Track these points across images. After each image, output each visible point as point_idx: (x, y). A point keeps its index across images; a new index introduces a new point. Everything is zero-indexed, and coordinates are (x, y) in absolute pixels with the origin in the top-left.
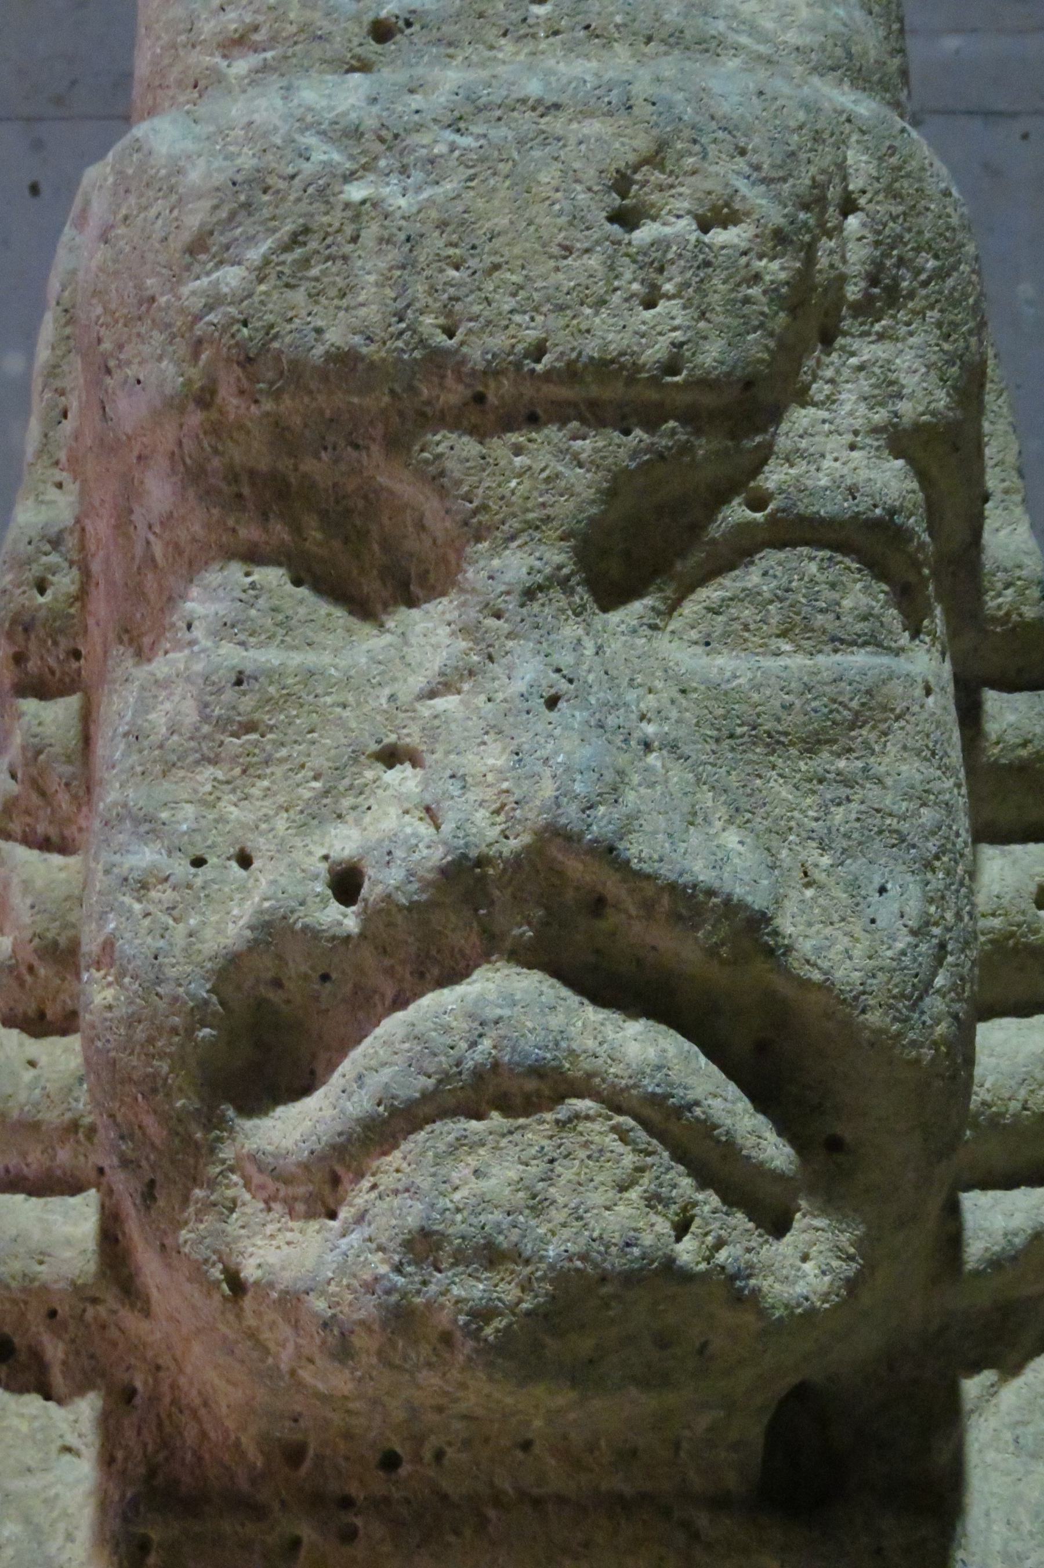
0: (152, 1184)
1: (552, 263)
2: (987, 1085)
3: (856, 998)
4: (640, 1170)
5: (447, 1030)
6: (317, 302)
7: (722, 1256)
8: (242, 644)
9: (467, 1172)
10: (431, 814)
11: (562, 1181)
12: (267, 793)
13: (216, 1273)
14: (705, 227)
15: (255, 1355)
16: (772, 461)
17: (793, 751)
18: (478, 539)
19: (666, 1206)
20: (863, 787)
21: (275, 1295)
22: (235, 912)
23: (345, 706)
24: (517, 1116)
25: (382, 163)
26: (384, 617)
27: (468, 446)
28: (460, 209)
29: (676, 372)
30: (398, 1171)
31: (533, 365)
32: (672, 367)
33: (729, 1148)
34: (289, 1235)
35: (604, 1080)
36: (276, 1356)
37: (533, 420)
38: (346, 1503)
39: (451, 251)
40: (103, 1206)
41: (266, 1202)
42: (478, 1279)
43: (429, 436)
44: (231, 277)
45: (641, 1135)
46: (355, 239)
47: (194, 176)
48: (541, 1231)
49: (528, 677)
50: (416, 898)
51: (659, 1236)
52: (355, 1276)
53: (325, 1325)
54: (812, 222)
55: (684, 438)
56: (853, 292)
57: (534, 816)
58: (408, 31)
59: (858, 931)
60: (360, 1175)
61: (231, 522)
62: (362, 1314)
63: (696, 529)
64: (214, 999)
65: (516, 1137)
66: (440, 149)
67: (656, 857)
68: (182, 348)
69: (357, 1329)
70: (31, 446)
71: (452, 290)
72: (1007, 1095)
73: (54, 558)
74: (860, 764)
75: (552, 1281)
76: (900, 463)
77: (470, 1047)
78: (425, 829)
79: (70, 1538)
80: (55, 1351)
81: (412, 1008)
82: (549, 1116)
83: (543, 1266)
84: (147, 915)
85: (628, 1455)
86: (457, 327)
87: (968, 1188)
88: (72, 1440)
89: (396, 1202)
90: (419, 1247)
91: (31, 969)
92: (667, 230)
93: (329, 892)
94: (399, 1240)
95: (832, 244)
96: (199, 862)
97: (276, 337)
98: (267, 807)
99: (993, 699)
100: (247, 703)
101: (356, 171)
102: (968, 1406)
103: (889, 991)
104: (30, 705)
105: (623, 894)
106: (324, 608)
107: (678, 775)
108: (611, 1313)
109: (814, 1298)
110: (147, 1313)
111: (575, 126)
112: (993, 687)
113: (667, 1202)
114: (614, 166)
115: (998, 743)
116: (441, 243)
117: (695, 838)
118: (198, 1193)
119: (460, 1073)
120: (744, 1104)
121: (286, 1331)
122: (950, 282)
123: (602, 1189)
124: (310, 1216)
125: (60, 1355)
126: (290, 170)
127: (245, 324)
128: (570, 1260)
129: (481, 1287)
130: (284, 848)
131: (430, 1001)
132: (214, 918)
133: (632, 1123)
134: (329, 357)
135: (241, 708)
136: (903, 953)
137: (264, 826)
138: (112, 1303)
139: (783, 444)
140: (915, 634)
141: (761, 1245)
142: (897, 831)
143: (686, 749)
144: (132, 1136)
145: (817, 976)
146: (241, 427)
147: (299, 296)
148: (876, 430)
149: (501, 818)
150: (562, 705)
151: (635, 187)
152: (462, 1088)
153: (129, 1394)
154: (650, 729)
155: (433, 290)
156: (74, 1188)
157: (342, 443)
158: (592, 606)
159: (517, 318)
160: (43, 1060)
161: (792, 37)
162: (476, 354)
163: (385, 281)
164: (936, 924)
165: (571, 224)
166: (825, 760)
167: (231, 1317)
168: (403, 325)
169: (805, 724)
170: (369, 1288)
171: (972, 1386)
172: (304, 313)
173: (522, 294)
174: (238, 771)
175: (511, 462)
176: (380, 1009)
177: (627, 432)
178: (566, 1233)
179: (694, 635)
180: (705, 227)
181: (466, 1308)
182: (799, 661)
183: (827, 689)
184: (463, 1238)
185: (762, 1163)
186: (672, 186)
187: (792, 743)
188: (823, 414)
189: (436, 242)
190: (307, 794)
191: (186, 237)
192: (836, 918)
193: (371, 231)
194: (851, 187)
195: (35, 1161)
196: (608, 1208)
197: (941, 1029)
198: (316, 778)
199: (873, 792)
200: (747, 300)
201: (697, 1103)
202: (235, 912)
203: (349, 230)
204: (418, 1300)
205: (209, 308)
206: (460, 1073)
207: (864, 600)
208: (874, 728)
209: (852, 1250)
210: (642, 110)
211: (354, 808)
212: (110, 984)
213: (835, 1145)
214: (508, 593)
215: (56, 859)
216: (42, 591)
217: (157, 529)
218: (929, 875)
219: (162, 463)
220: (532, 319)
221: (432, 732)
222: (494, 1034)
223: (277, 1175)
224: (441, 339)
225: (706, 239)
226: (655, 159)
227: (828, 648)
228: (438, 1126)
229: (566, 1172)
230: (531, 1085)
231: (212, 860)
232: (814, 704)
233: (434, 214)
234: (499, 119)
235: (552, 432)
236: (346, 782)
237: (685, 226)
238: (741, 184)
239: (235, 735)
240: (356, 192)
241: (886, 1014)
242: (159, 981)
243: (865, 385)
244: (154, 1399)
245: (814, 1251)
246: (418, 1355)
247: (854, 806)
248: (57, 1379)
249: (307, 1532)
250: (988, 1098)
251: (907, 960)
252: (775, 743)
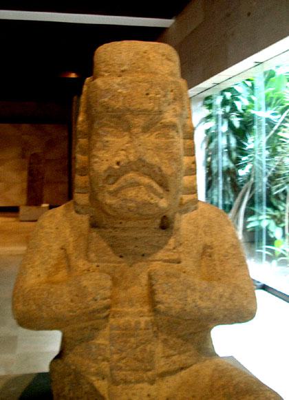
240: (119, 91)
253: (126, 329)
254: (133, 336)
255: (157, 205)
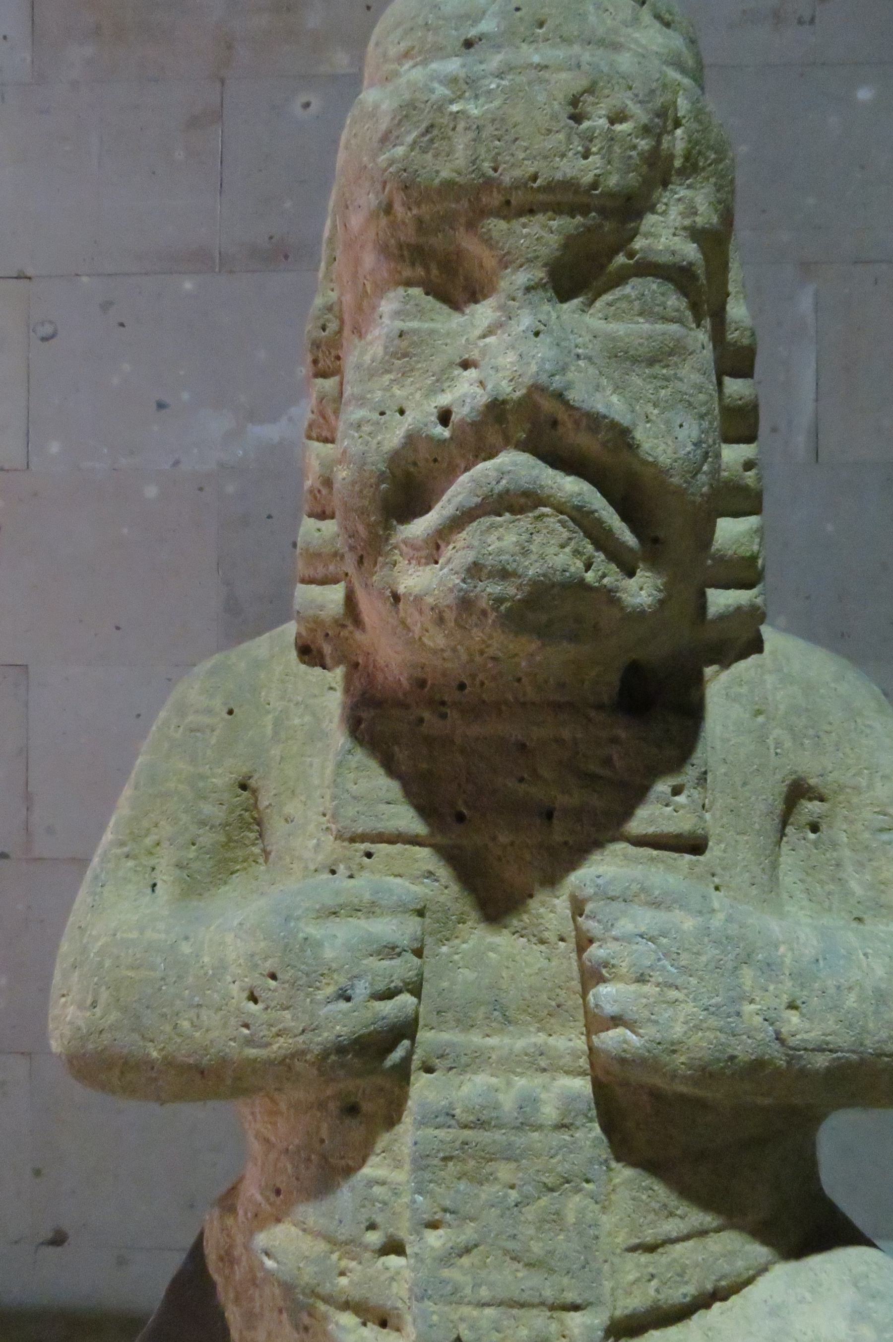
0: (361, 557)
1: (543, 137)
2: (719, 542)
3: (668, 470)
4: (570, 539)
5: (487, 476)
6: (437, 159)
7: (605, 581)
8: (403, 320)
9: (495, 538)
10: (482, 384)
11: (536, 542)
12: (412, 383)
13: (388, 593)
14: (612, 122)
15: (405, 632)
16: (638, 237)
17: (643, 365)
18: (506, 268)
19: (581, 555)
20: (673, 382)
21: (411, 598)
22: (398, 432)
23: (446, 345)
24: (516, 515)
25: (467, 94)
26: (465, 309)
27: (502, 225)
28: (501, 112)
29: (596, 189)
30: (464, 540)
31: (532, 184)
32: (594, 185)
33: (609, 532)
34: (418, 573)
35: (555, 499)
36: (413, 632)
37: (531, 212)
38: (443, 703)
39: (496, 133)
40: (347, 587)
41: (409, 561)
42: (499, 585)
43: (485, 221)
44: (400, 151)
45: (571, 524)
46: (454, 129)
47: (384, 107)
48: (526, 563)
49: (527, 324)
50: (475, 419)
51: (578, 568)
52: (445, 586)
53: (432, 609)
54: (661, 124)
55: (599, 221)
56: (678, 163)
57: (527, 381)
58: (480, 43)
59: (670, 443)
60: (448, 544)
61: (399, 269)
62: (448, 602)
63: (603, 267)
64: (388, 471)
65: (516, 523)
66: (493, 86)
67: (581, 400)
68: (379, 187)
69: (446, 609)
70: (321, 274)
71: (496, 150)
72: (727, 547)
73: (330, 316)
74: (672, 372)
75: (530, 585)
76: (695, 245)
77: (497, 483)
78: (480, 391)
79: (331, 721)
80: (327, 649)
81: (472, 471)
82: (530, 515)
83: (527, 579)
84: (361, 437)
85: (562, 686)
86: (498, 168)
87: (710, 587)
88: (334, 685)
89: (465, 552)
90: (473, 571)
91: (319, 491)
92: (595, 123)
93: (438, 422)
94: (464, 568)
95: (670, 138)
96: (382, 414)
97: (418, 176)
98: (412, 389)
99: (727, 380)
100: (404, 344)
101: (456, 99)
102: (706, 678)
103: (683, 468)
104: (320, 381)
105: (566, 417)
106: (438, 305)
107: (592, 371)
108: (556, 602)
109: (645, 606)
110: (364, 630)
111: (554, 75)
112: (727, 375)
113: (583, 554)
114: (572, 93)
115: (729, 397)
116: (492, 129)
117: (598, 395)
118: (380, 559)
119: (492, 495)
120: (616, 517)
121: (416, 615)
122: (721, 166)
123: (553, 546)
124: (427, 564)
125: (330, 652)
126: (426, 99)
127: (405, 170)
128: (538, 576)
129: (499, 588)
130: (419, 404)
131: (481, 466)
132: (388, 436)
133: (568, 519)
134: (442, 184)
135: (402, 346)
136: (689, 453)
137: (410, 397)
138: (351, 628)
139: (643, 228)
140: (698, 326)
141: (622, 579)
142: (688, 401)
143: (596, 361)
144: (353, 536)
145: (651, 459)
146: (404, 223)
147: (429, 156)
148: (685, 228)
149: (513, 383)
150: (541, 335)
151: (581, 104)
152: (493, 502)
153: (356, 665)
154: (580, 351)
155: (488, 151)
156: (336, 581)
157: (447, 228)
158: (555, 299)
159: (526, 162)
160: (323, 528)
161: (655, 48)
162: (507, 180)
163: (467, 147)
164: (704, 443)
165: (551, 119)
166: (657, 369)
167: (394, 613)
168: (475, 167)
169: (649, 353)
170: (451, 590)
171: (709, 671)
172: (431, 164)
173: (528, 152)
174: (400, 375)
175: (521, 232)
176: (459, 474)
177: (573, 217)
178: (538, 564)
179: (600, 315)
180: (612, 122)
181: (493, 597)
182: (647, 326)
183: (660, 337)
184: (492, 566)
185: (624, 542)
186: (598, 103)
187: (642, 361)
188: (662, 219)
189: (489, 130)
190: (429, 382)
191: (379, 135)
192: (660, 436)
193: (461, 125)
194: (679, 115)
195: (321, 572)
196: (555, 555)
197: (705, 489)
198: (433, 376)
199: (679, 384)
200: (630, 157)
201: (596, 511)
202: (398, 432)
203: (451, 126)
204: (472, 594)
205: (390, 165)
206: (492, 495)
207: (677, 303)
208: (679, 356)
209: (662, 588)
210: (586, 67)
211: (449, 387)
212: (344, 470)
213: (656, 540)
214: (518, 289)
215: (330, 446)
216: (324, 329)
217: (368, 277)
218: (702, 422)
219: (370, 246)
220: (533, 163)
221: (484, 352)
222: (508, 477)
223: (415, 548)
224: (491, 173)
225: (612, 128)
226: (591, 90)
227: (660, 321)
228: (482, 519)
229: (537, 539)
230: (522, 501)
231: (388, 412)
232: (653, 344)
233: (489, 116)
234: (520, 73)
235: (540, 217)
236: (446, 376)
237: (603, 122)
238: (629, 102)
239: (398, 359)
240: (455, 108)
241: (681, 478)
242: (365, 464)
243: (681, 207)
244: (366, 667)
245: (645, 586)
246: (472, 620)
247: (669, 389)
248: (328, 661)
249: (427, 715)
250: (719, 547)
251: (691, 456)
252: (635, 360)
253: (481, 1124)
254: (509, 1155)
255: (610, 596)
